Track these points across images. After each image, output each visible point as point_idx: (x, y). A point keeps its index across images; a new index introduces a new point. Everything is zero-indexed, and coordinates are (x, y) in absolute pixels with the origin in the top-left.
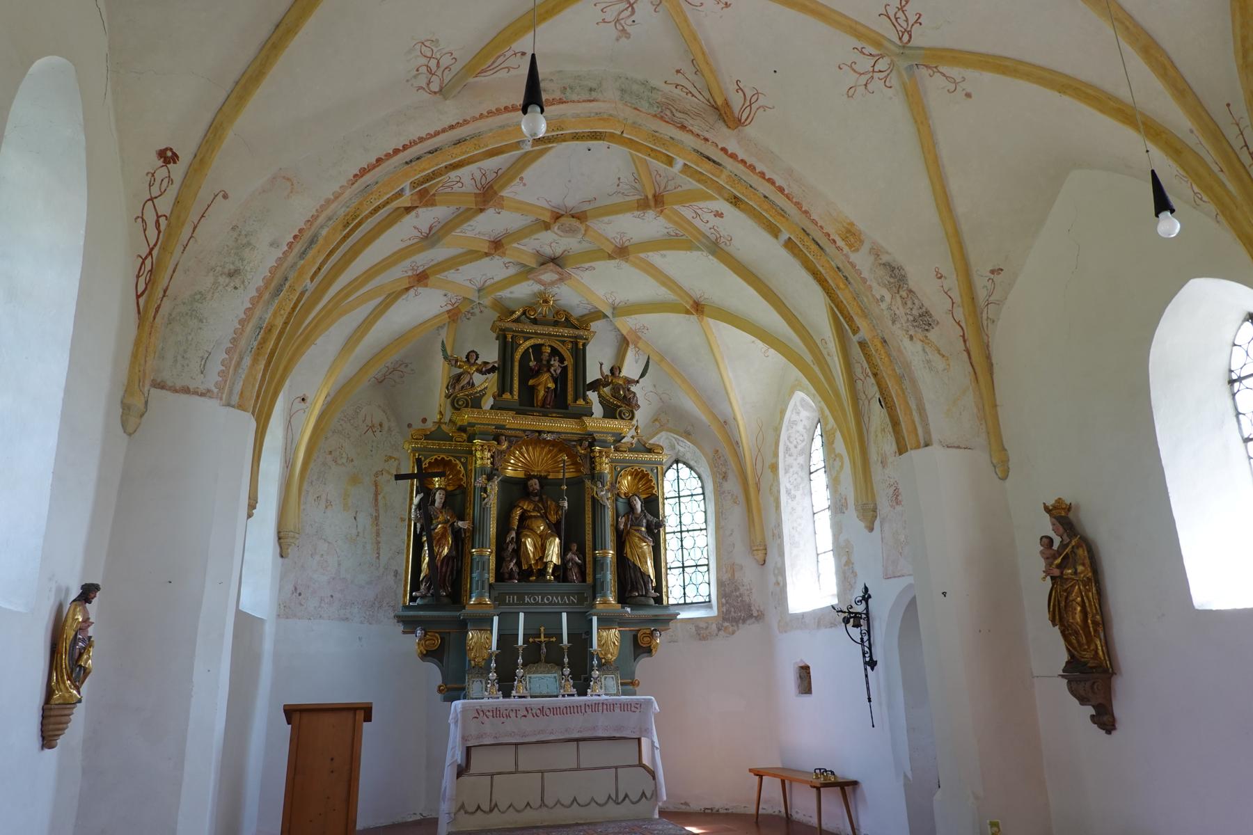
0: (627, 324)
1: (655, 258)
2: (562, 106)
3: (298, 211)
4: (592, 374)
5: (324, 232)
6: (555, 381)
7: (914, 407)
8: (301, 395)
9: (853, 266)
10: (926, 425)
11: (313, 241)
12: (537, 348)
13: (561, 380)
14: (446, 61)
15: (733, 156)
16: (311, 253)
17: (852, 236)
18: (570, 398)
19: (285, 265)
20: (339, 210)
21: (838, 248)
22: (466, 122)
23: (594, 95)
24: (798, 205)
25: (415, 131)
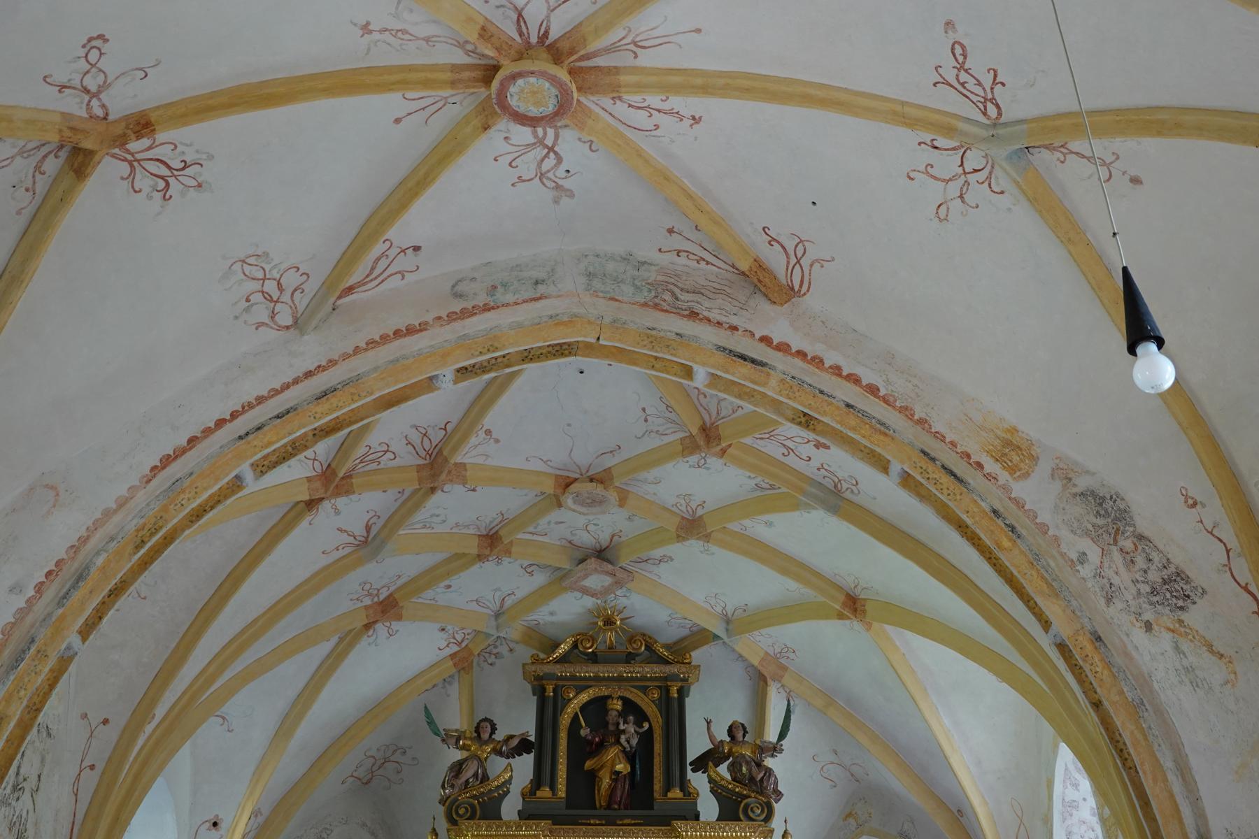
0: (759, 644)
1: (757, 527)
2: (488, 315)
3: (59, 533)
4: (696, 745)
5: (100, 561)
6: (630, 757)
7: (1168, 764)
8: (211, 817)
9: (1019, 504)
10: (1196, 802)
11: (80, 577)
12: (599, 703)
13: (641, 756)
14: (291, 280)
15: (783, 348)
16: (77, 596)
17: (1014, 451)
18: (658, 786)
19: (29, 620)
20: (127, 522)
21: (989, 477)
22: (332, 363)
23: (541, 289)
24: (906, 411)
25: (250, 389)
